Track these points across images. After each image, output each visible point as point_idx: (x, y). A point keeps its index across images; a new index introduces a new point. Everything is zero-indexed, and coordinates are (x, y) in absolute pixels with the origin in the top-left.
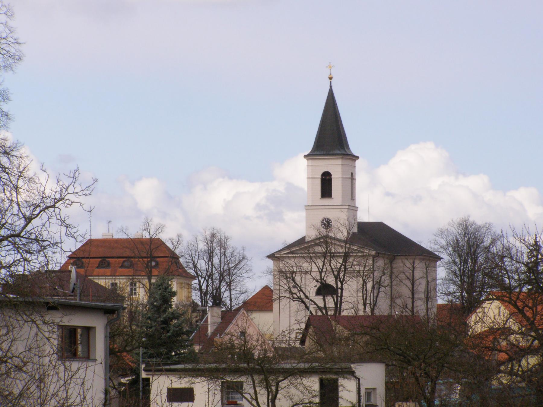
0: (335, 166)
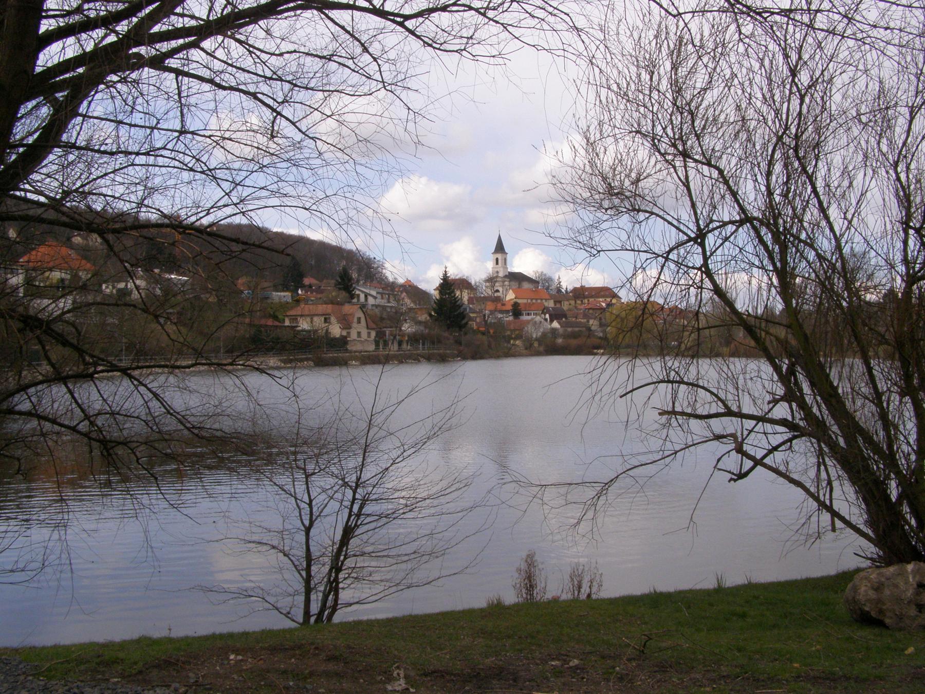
0: (499, 256)
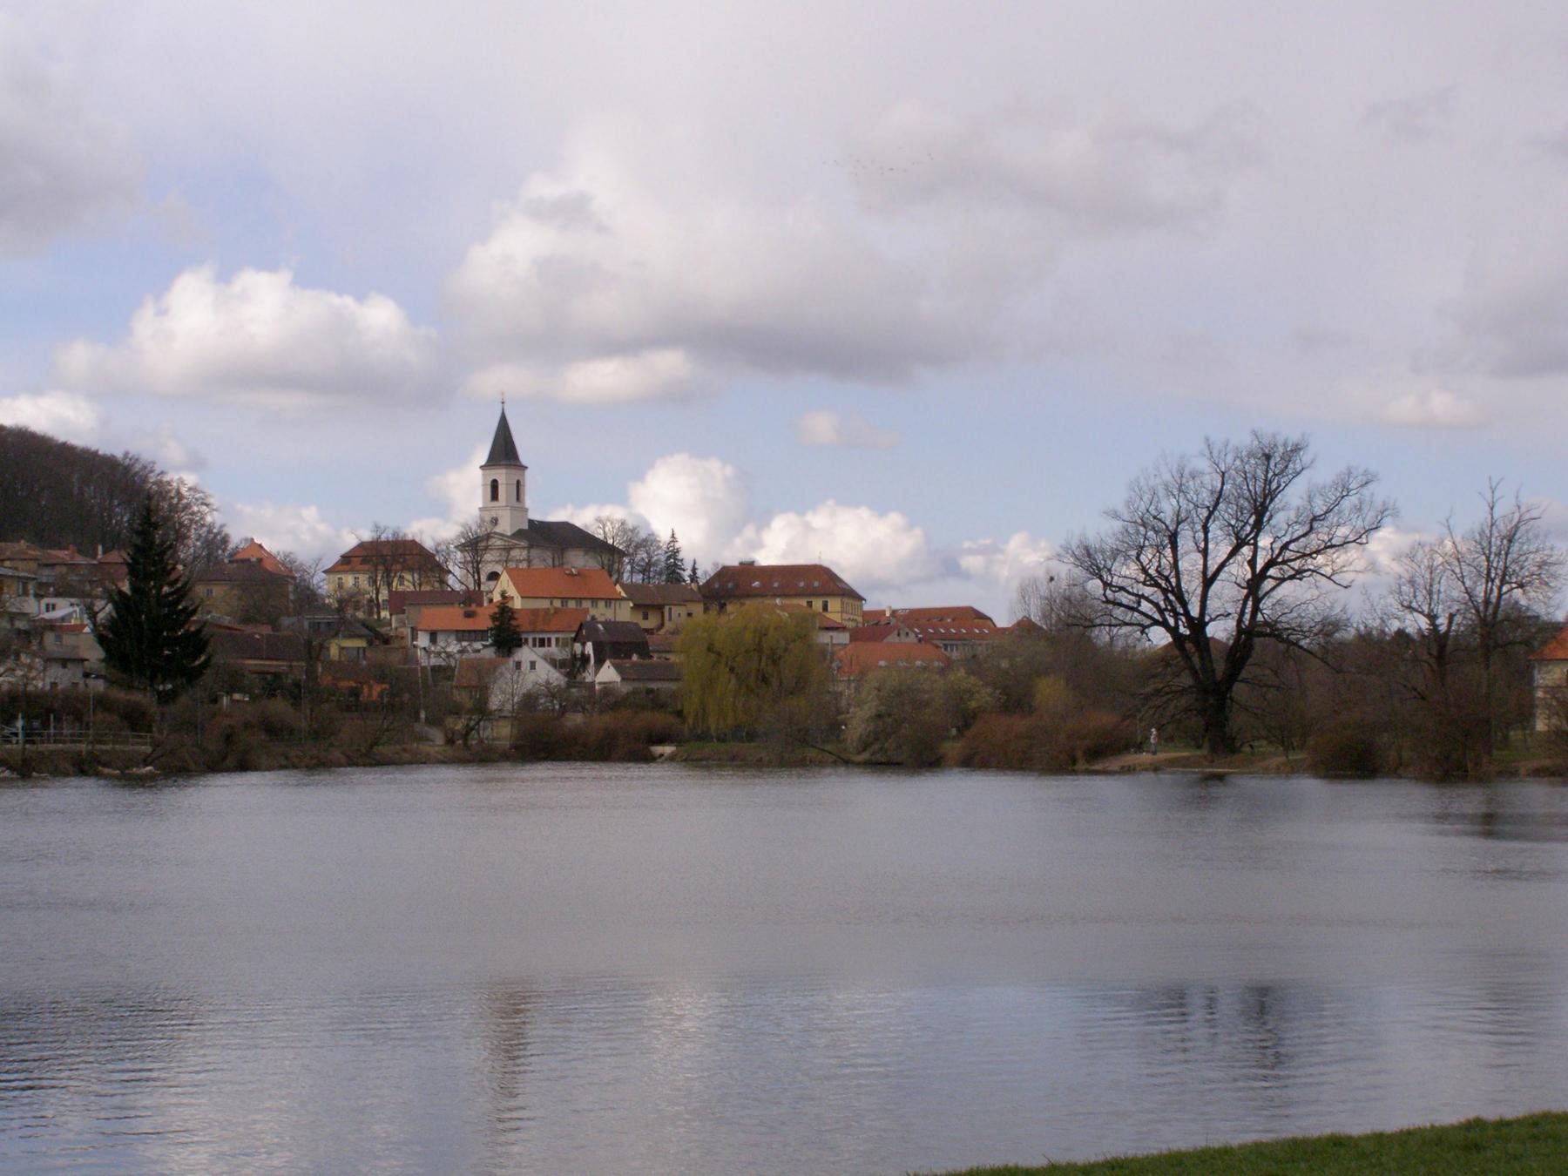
0: (501, 475)
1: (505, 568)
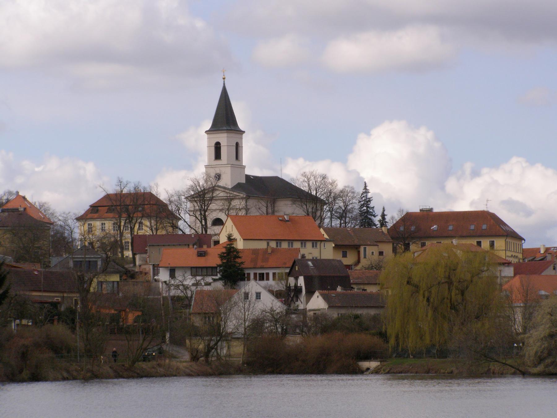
0: (223, 138)
1: (228, 216)
